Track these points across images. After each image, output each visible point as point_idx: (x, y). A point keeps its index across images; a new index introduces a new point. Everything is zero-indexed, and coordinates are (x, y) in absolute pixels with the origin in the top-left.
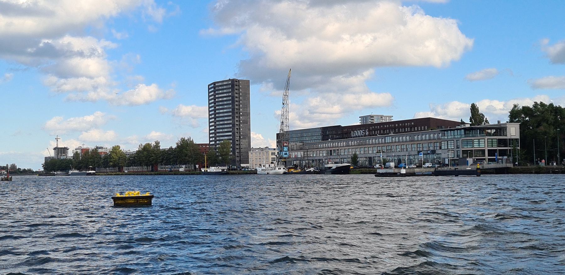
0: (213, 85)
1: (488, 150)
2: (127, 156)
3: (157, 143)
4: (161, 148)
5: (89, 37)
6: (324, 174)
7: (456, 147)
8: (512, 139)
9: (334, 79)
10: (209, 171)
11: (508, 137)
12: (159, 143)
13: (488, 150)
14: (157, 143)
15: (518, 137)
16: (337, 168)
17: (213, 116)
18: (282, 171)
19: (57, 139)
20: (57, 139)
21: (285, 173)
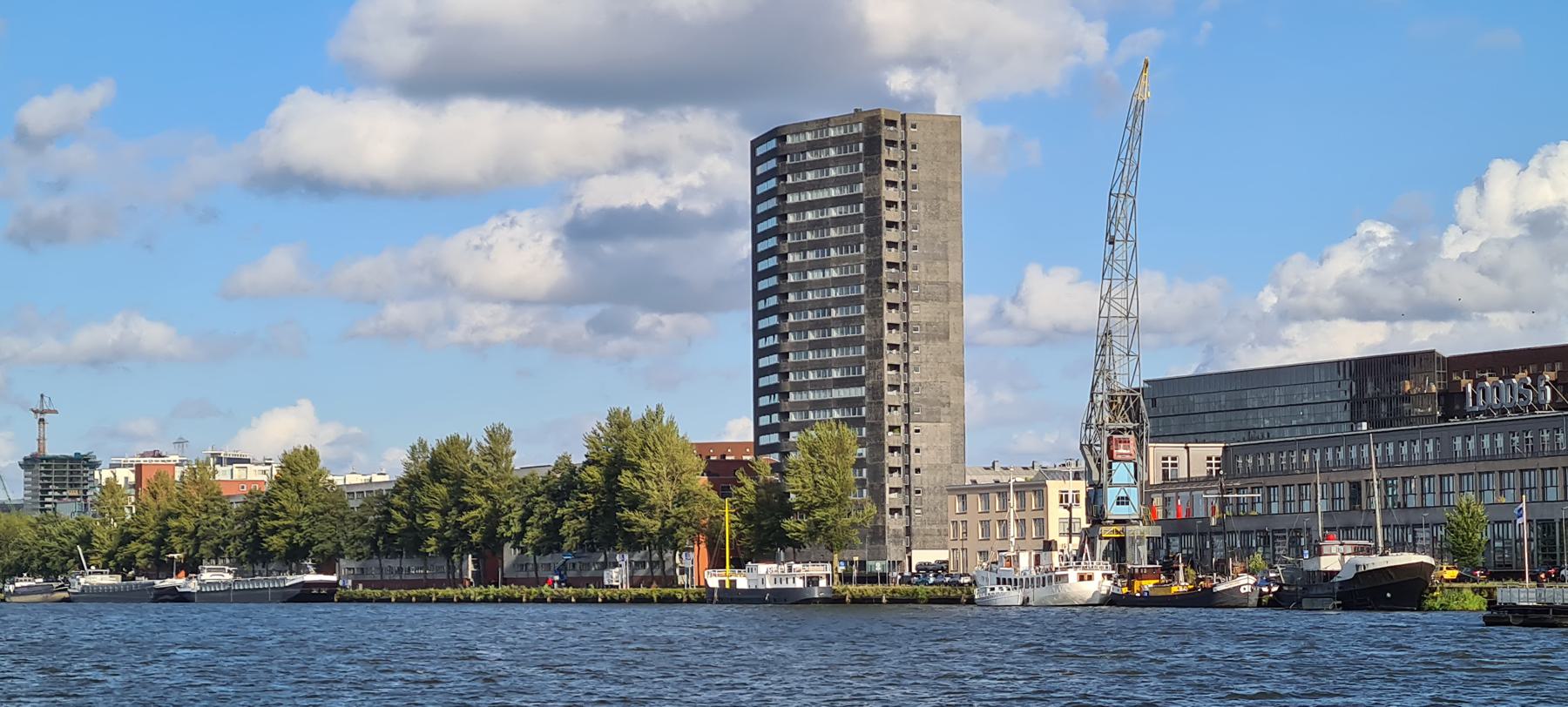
0: (772, 144)
2: (354, 503)
3: (499, 438)
4: (518, 462)
5: (663, 112)
6: (1299, 607)
9: (1489, 315)
10: (742, 583)
12: (507, 438)
14: (499, 438)
16: (1364, 576)
17: (773, 301)
18: (1454, 574)
19: (41, 414)
20: (41, 414)
21: (1111, 600)
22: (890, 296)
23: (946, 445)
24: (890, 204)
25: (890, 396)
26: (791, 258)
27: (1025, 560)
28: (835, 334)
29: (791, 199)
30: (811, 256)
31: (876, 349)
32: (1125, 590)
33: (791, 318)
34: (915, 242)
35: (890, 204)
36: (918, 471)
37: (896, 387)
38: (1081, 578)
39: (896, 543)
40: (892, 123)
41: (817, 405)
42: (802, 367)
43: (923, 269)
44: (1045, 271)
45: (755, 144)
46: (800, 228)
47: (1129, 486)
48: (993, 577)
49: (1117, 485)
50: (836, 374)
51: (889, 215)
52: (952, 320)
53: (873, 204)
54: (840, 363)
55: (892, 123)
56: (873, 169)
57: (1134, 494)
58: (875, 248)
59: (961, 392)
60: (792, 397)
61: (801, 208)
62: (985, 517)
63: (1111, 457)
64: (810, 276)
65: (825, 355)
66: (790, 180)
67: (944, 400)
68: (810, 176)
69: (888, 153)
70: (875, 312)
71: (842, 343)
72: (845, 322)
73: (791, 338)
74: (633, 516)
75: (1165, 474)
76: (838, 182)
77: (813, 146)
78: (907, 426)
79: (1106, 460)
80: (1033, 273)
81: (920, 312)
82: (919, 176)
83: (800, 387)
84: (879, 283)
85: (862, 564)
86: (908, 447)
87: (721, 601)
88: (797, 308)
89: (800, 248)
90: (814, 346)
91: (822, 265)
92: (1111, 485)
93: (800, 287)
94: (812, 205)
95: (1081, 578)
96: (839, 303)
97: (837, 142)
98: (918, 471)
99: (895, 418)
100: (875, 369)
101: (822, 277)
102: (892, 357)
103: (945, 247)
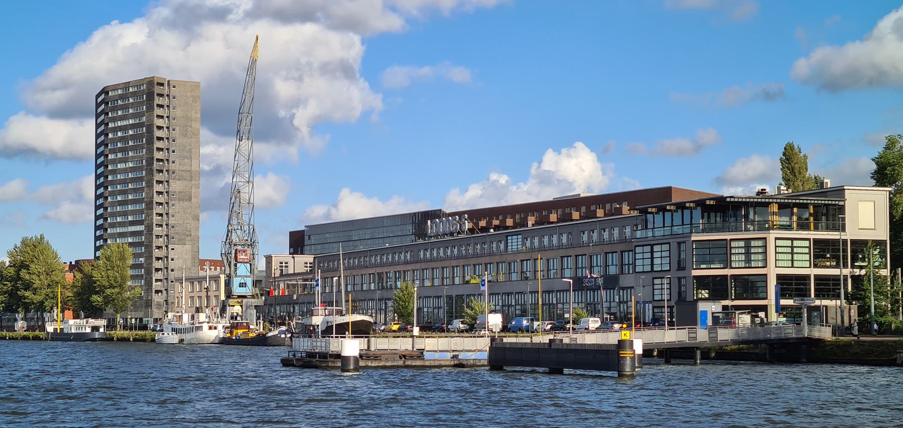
0: (103, 96)
1: (780, 277)
7: (675, 266)
8: (864, 243)
11: (850, 234)
13: (780, 277)
15: (883, 233)
21: (224, 341)
22: (158, 177)
23: (189, 257)
24: (160, 128)
25: (157, 230)
26: (110, 157)
27: (186, 318)
28: (130, 197)
29: (111, 125)
30: (120, 155)
31: (150, 205)
32: (229, 335)
33: (110, 189)
34: (173, 148)
35: (160, 128)
36: (172, 270)
37: (161, 226)
38: (210, 328)
39: (158, 309)
40: (162, 85)
41: (122, 235)
42: (114, 215)
43: (177, 163)
44: (351, 192)
45: (98, 96)
46: (115, 141)
47: (246, 277)
48: (170, 327)
49: (240, 276)
50: (130, 218)
51: (158, 133)
52: (193, 190)
53: (150, 128)
54: (133, 213)
55: (162, 85)
56: (150, 109)
57: (249, 282)
58: (150, 151)
59: (197, 229)
60: (109, 231)
61: (115, 130)
62: (192, 295)
63: (236, 260)
64: (119, 166)
65: (125, 208)
66: (110, 115)
67: (188, 233)
68: (120, 113)
69: (157, 101)
70: (150, 185)
71: (134, 202)
72: (135, 191)
73: (109, 199)
74: (27, 294)
75: (282, 270)
76: (133, 116)
77: (122, 97)
78: (167, 246)
79: (233, 262)
80: (345, 192)
81: (176, 186)
82: (177, 112)
83: (113, 225)
84: (152, 170)
85: (141, 320)
86: (167, 257)
87: (53, 339)
88: (113, 183)
89: (113, 151)
90: (121, 203)
91: (124, 160)
92: (236, 276)
93: (114, 172)
94: (121, 128)
95: (210, 328)
96: (133, 180)
97: (134, 94)
98: (172, 270)
99: (160, 242)
100: (149, 215)
101: (124, 166)
102: (157, 209)
103: (190, 151)
